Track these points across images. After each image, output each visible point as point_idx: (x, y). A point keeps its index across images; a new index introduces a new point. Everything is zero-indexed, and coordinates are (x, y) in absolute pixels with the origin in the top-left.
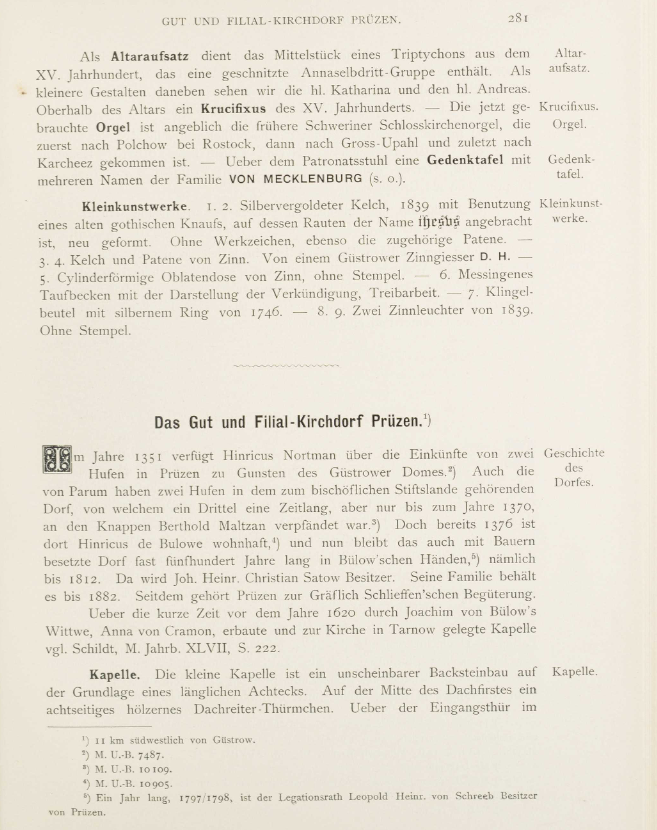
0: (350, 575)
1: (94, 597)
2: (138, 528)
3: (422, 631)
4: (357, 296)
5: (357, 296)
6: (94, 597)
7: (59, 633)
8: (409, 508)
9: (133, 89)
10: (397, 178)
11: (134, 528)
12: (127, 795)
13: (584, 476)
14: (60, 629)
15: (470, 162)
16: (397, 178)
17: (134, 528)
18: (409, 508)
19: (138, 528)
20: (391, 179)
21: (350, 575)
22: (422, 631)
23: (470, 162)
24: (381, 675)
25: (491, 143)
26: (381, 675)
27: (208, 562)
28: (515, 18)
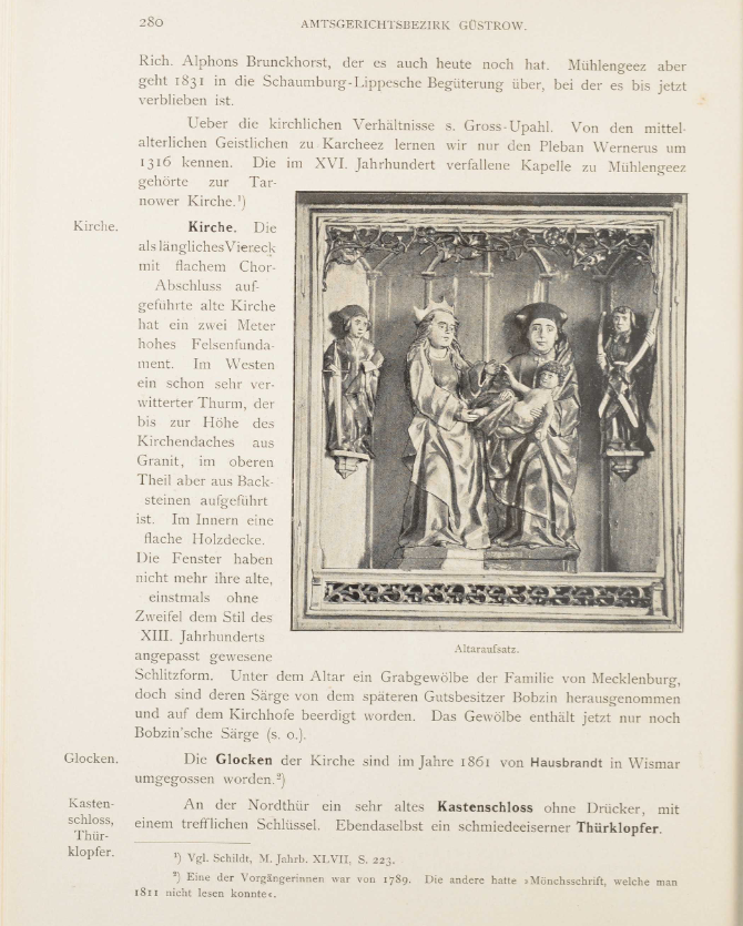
0: (140, 729)
1: (467, 762)
2: (386, 84)
3: (151, 202)
4: (676, 683)
5: (676, 683)
6: (467, 762)
7: (643, 765)
8: (142, 423)
9: (156, 139)
10: (297, 735)
11: (382, 84)
12: (189, 631)
13: (104, 845)
14: (644, 760)
15: (613, 830)
16: (297, 735)
17: (382, 84)
18: (142, 423)
19: (386, 84)
20: (291, 736)
21: (140, 729)
22: (151, 202)
23: (613, 830)
24: (146, 824)
25: (606, 718)
26: (146, 824)
27: (171, 501)
28: (148, 21)
